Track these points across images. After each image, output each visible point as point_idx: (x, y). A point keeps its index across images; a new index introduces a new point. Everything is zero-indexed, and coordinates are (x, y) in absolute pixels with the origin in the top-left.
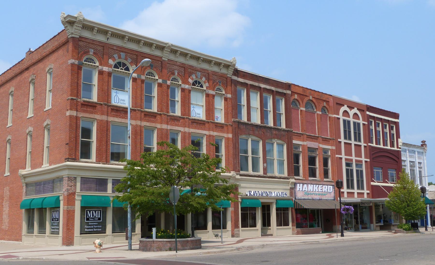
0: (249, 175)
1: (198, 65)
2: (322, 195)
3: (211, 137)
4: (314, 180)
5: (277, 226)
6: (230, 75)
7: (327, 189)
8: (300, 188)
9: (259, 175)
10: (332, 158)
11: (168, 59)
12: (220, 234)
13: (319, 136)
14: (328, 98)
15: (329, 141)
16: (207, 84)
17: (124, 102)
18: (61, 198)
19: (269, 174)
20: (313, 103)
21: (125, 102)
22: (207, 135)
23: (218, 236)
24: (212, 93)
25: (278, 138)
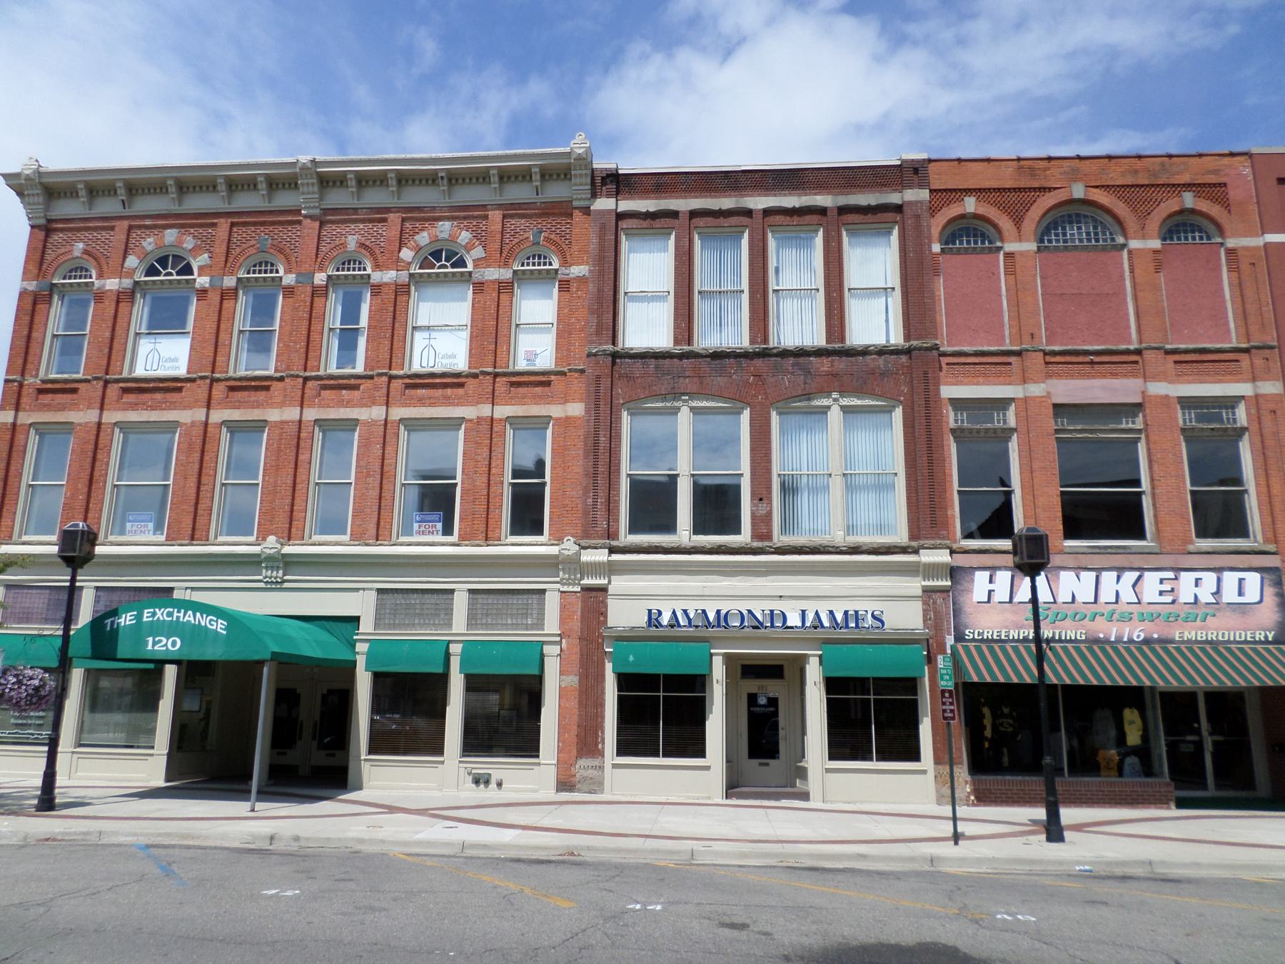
0: (663, 548)
1: (495, 196)
2: (1173, 618)
3: (483, 423)
4: (1109, 551)
5: (832, 757)
6: (584, 199)
7: (1214, 590)
8: (990, 592)
9: (720, 546)
10: (1257, 439)
11: (321, 209)
12: (496, 775)
13: (915, 343)
14: (1216, 172)
15: (1238, 361)
16: (478, 252)
17: (174, 364)
18: (549, 650)
19: (779, 539)
20: (1099, 211)
21: (177, 364)
22: (471, 421)
23: (487, 782)
24: (496, 276)
25: (843, 393)
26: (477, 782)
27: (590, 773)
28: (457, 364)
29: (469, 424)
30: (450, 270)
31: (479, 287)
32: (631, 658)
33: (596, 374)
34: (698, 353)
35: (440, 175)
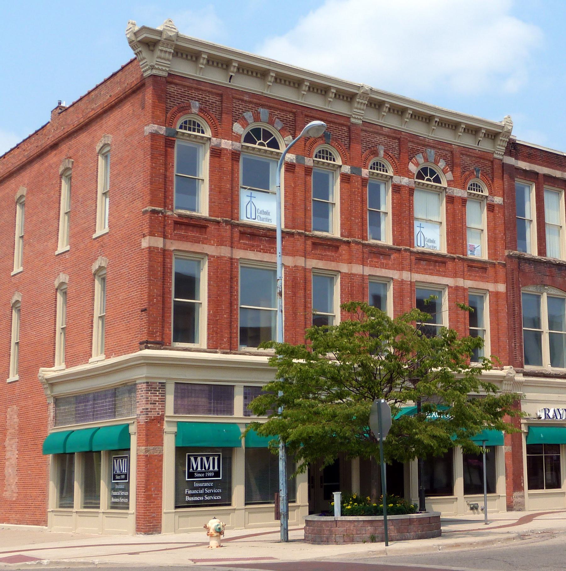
6: (500, 154)
16: (449, 175)
22: (451, 287)
24: (459, 195)
26: (472, 509)
27: (519, 499)
28: (436, 247)
29: (450, 290)
30: (266, 148)
31: (451, 200)
32: (542, 436)
33: (512, 268)
34: (552, 262)
35: (203, 56)
